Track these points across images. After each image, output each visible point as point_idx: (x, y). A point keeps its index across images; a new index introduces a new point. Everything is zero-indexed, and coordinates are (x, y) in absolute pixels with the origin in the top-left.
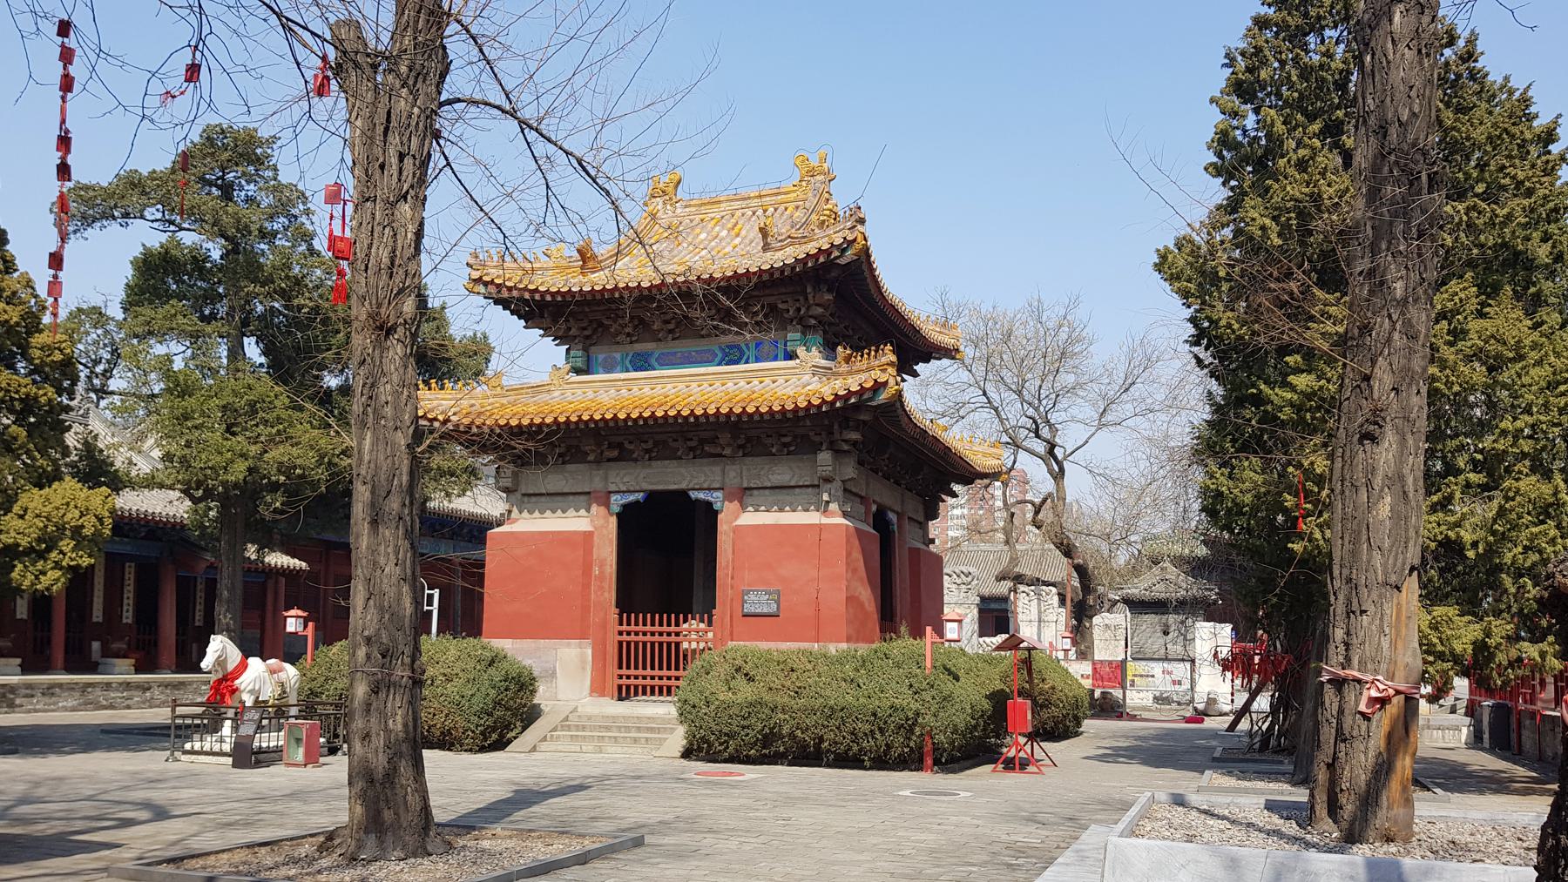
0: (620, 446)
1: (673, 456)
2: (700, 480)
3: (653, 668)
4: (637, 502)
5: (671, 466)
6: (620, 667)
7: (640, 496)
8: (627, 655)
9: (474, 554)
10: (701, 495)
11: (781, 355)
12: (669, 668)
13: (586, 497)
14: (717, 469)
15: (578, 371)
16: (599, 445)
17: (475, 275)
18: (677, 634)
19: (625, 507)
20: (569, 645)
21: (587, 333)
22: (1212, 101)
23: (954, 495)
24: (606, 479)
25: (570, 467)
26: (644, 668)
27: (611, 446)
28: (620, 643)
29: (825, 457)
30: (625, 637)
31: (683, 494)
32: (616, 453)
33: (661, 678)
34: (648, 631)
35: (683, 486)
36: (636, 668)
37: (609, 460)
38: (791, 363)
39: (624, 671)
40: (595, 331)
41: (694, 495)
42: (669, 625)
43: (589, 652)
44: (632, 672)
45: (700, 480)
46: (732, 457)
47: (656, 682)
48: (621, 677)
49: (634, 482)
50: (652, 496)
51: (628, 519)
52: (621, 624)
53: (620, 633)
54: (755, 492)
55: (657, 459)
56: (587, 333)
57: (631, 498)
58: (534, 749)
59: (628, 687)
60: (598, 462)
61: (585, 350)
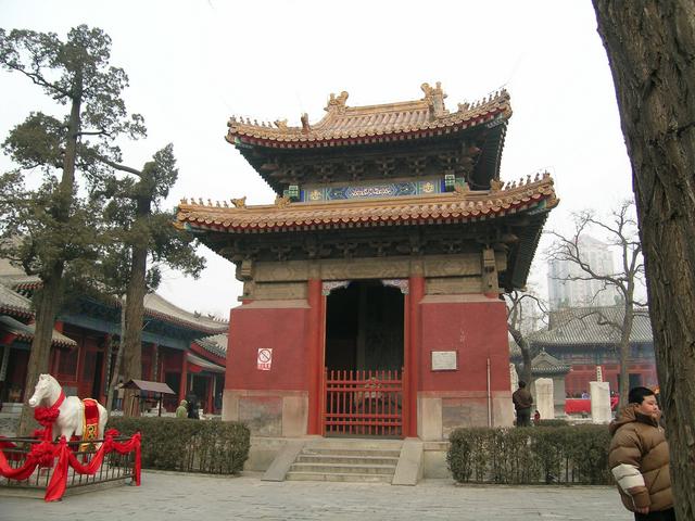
0: (332, 247)
1: (374, 254)
2: (392, 271)
3: (341, 412)
4: (342, 288)
5: (369, 261)
9: (156, 348)
10: (392, 283)
12: (348, 412)
14: (405, 263)
16: (318, 245)
17: (233, 131)
18: (354, 386)
19: (334, 292)
20: (292, 395)
21: (300, 175)
22: (197, 277)
24: (320, 270)
25: (292, 263)
27: (325, 247)
29: (488, 254)
30: (332, 389)
31: (378, 281)
32: (329, 252)
33: (341, 419)
35: (379, 276)
36: (335, 412)
37: (323, 258)
38: (451, 194)
39: (332, 415)
40: (306, 174)
41: (386, 283)
42: (336, 379)
43: (307, 400)
44: (344, 415)
45: (392, 271)
46: (417, 254)
47: (337, 422)
48: (329, 419)
49: (334, 277)
50: (354, 284)
52: (329, 378)
53: (329, 386)
54: (433, 281)
55: (358, 257)
56: (300, 175)
57: (338, 285)
58: (286, 478)
60: (314, 259)
61: (300, 186)
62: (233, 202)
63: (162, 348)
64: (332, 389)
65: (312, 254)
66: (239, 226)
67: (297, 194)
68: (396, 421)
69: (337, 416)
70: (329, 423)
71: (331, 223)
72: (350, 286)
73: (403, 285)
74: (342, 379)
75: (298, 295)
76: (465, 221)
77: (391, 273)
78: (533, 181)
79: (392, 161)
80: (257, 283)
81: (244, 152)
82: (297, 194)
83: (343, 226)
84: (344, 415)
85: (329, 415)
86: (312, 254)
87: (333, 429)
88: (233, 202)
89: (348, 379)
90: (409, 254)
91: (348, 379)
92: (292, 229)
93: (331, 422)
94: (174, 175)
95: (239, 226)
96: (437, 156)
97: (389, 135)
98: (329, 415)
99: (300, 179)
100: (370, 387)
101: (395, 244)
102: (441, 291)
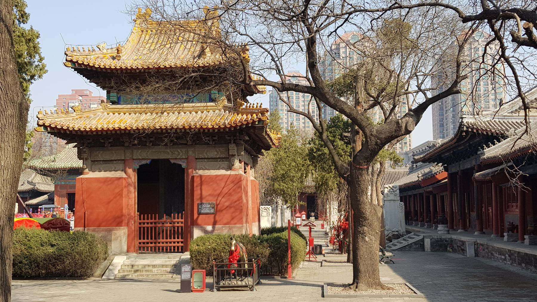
4: (147, 164)
6: (140, 239)
7: (148, 162)
8: (143, 233)
11: (208, 99)
12: (144, 239)
13: (124, 164)
14: (184, 150)
15: (114, 103)
23: (263, 155)
26: (148, 239)
28: (140, 228)
30: (142, 225)
31: (168, 160)
34: (148, 223)
36: (170, 238)
39: (142, 241)
41: (172, 161)
42: (144, 219)
50: (153, 161)
51: (142, 172)
52: (140, 219)
57: (144, 162)
59: (174, 247)
65: (127, 144)
66: (62, 128)
69: (147, 240)
70: (140, 226)
71: (138, 129)
72: (151, 162)
74: (148, 239)
76: (222, 130)
78: (255, 107)
84: (146, 221)
85: (140, 221)
87: (142, 249)
89: (155, 219)
93: (142, 245)
95: (62, 128)
102: (208, 175)
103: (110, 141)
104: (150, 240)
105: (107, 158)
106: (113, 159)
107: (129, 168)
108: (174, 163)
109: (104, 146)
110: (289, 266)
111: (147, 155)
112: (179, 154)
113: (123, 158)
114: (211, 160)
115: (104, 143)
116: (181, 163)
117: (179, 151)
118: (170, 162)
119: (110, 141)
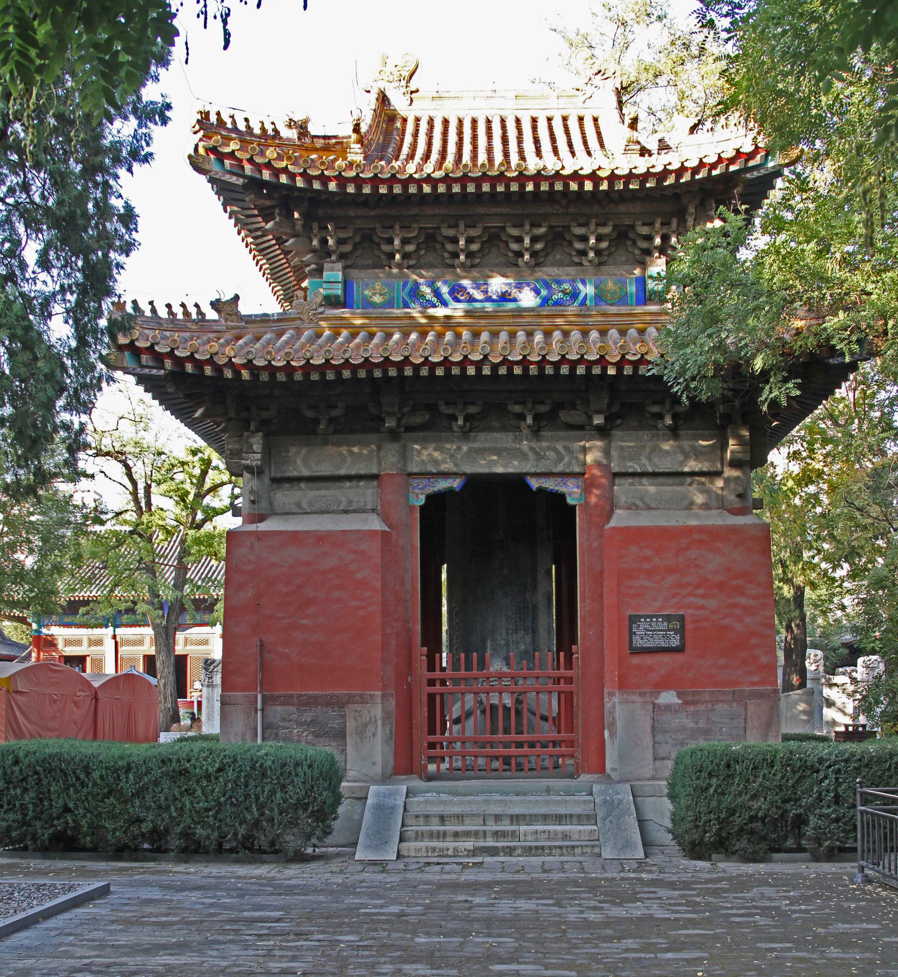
4: (450, 492)
7: (456, 484)
10: (549, 484)
31: (517, 482)
37: (409, 429)
56: (347, 248)
57: (442, 485)
62: (216, 305)
63: (633, 959)
64: (438, 688)
65: (390, 423)
67: (338, 291)
68: (569, 742)
70: (432, 689)
73: (572, 492)
75: (362, 510)
77: (573, 463)
79: (543, 230)
80: (274, 480)
81: (222, 188)
82: (338, 291)
83: (533, 370)
86: (390, 423)
88: (216, 305)
89: (468, 668)
90: (581, 428)
91: (468, 668)
92: (440, 372)
94: (129, 217)
96: (632, 227)
97: (546, 178)
98: (432, 738)
99: (342, 256)
100: (505, 672)
101: (559, 406)
103: (336, 413)
104: (501, 736)
105: (325, 469)
106: (343, 472)
107: (672, 446)
108: (541, 490)
109: (314, 433)
110: (227, 753)
111: (448, 461)
112: (560, 459)
113: (375, 471)
114: (661, 480)
115: (316, 421)
116: (562, 489)
117: (559, 447)
118: (528, 487)
119: (336, 413)
